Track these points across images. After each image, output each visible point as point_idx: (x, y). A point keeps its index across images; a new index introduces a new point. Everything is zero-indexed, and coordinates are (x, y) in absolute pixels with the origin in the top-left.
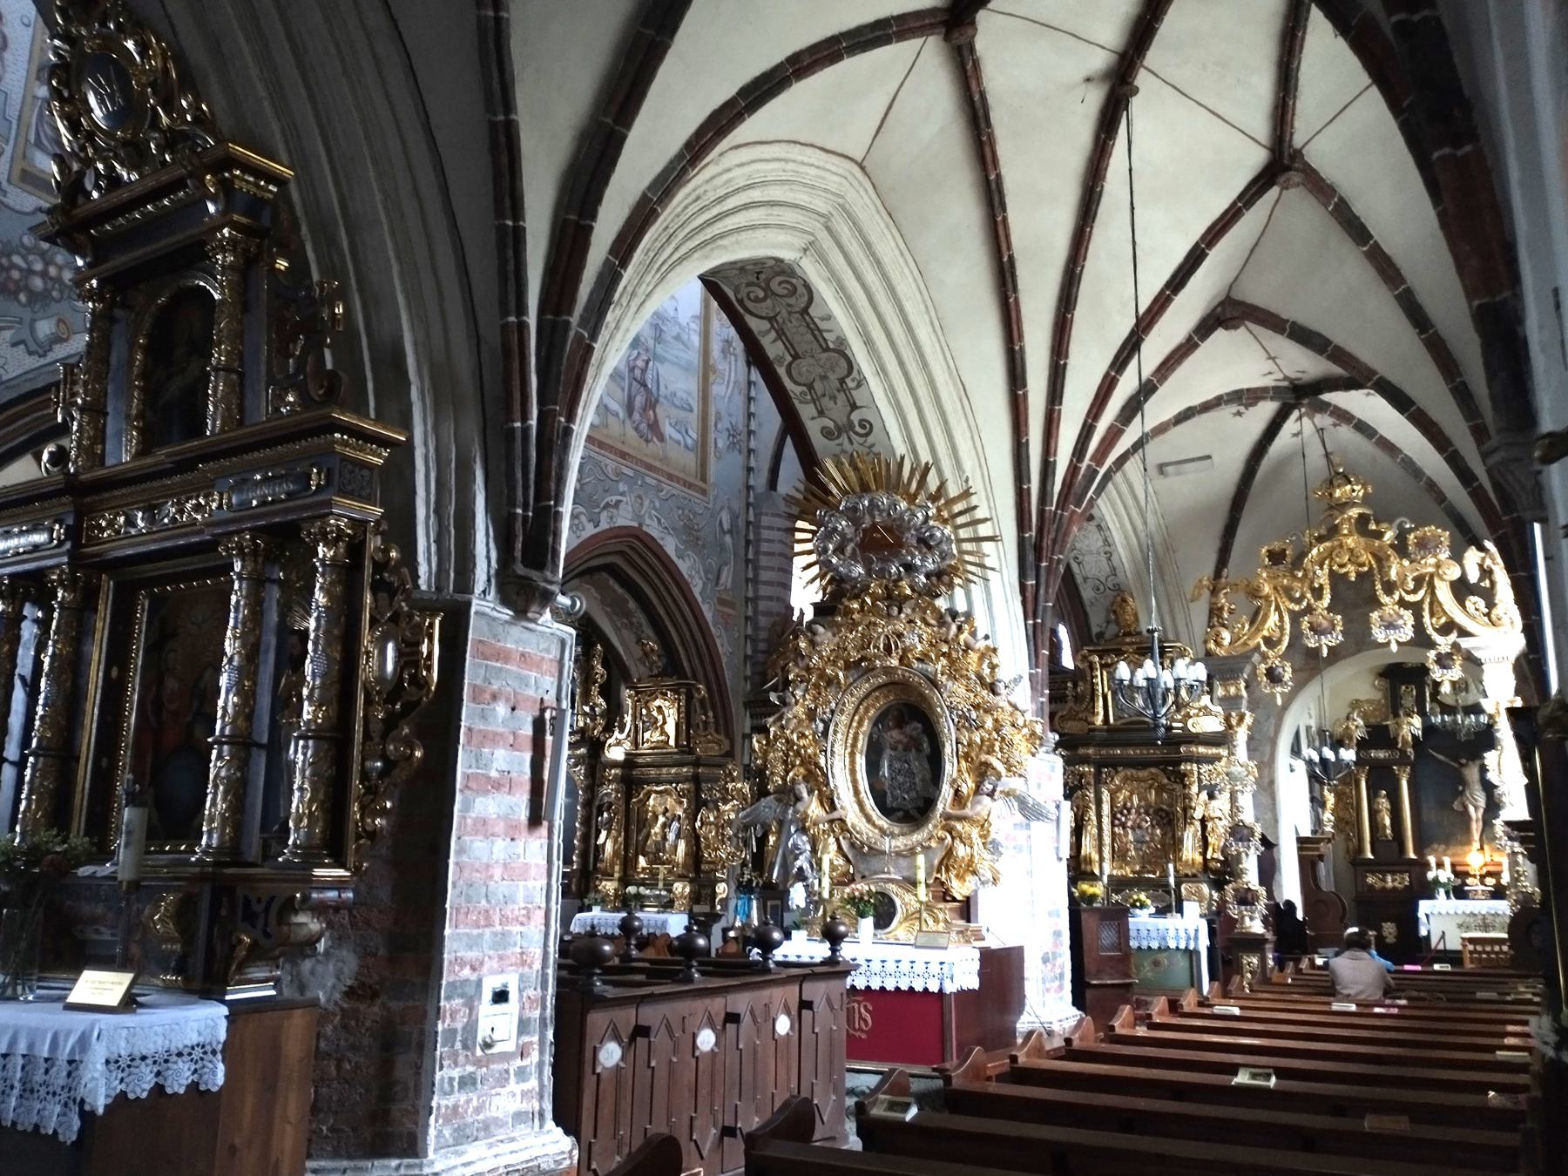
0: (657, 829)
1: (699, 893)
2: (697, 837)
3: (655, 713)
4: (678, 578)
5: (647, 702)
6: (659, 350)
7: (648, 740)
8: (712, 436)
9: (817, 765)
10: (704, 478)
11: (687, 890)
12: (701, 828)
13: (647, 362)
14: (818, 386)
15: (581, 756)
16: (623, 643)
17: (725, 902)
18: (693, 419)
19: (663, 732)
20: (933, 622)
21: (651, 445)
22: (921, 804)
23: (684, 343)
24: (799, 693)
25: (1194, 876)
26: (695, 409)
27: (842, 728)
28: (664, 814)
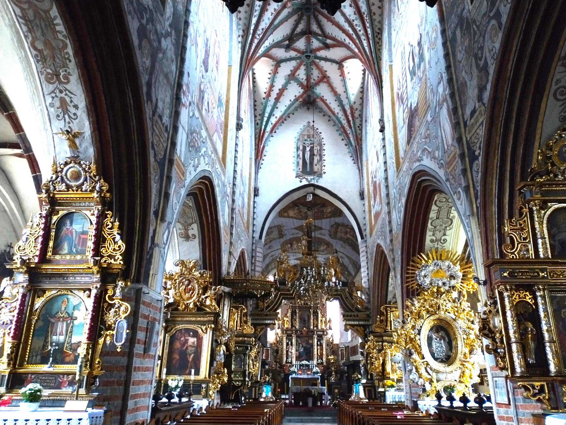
14: (438, 228)
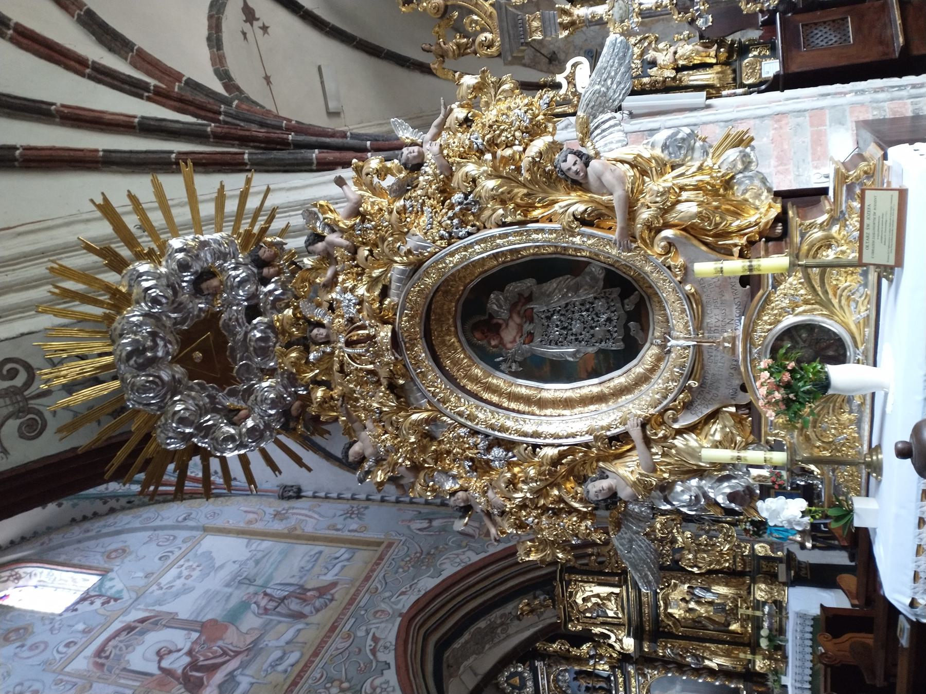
0: (702, 610)
1: (766, 573)
2: (710, 572)
3: (589, 605)
4: (458, 577)
5: (579, 611)
6: (259, 582)
7: (615, 613)
8: (346, 534)
9: (556, 462)
10: (379, 544)
11: (763, 586)
12: (699, 568)
13: (266, 594)
15: (637, 670)
16: (522, 631)
17: (774, 546)
18: (328, 550)
19: (608, 598)
20: (330, 273)
21: (336, 596)
22: (616, 292)
23: (264, 557)
24: (449, 485)
25: (734, 71)
26: (318, 549)
27: (501, 419)
28: (687, 602)
